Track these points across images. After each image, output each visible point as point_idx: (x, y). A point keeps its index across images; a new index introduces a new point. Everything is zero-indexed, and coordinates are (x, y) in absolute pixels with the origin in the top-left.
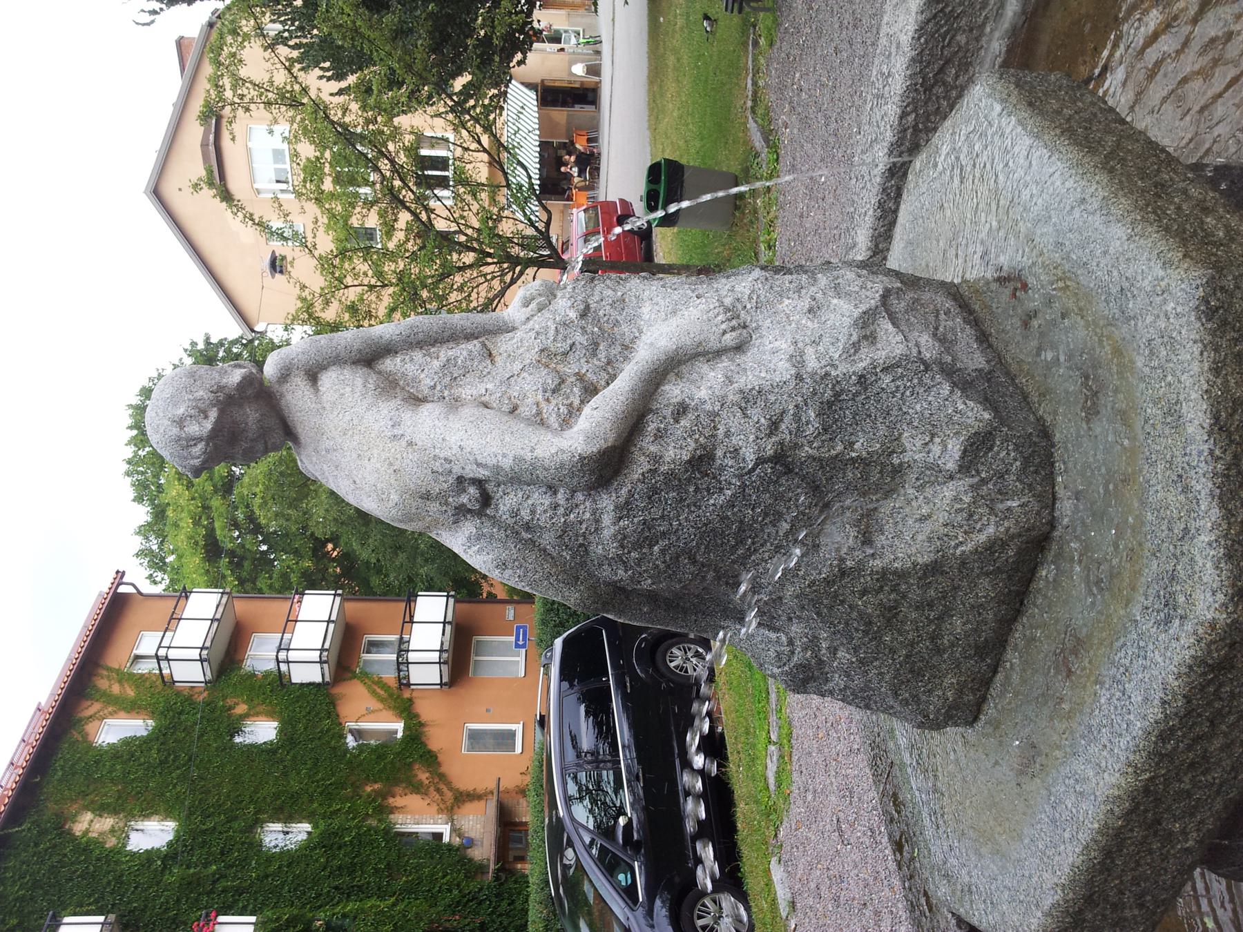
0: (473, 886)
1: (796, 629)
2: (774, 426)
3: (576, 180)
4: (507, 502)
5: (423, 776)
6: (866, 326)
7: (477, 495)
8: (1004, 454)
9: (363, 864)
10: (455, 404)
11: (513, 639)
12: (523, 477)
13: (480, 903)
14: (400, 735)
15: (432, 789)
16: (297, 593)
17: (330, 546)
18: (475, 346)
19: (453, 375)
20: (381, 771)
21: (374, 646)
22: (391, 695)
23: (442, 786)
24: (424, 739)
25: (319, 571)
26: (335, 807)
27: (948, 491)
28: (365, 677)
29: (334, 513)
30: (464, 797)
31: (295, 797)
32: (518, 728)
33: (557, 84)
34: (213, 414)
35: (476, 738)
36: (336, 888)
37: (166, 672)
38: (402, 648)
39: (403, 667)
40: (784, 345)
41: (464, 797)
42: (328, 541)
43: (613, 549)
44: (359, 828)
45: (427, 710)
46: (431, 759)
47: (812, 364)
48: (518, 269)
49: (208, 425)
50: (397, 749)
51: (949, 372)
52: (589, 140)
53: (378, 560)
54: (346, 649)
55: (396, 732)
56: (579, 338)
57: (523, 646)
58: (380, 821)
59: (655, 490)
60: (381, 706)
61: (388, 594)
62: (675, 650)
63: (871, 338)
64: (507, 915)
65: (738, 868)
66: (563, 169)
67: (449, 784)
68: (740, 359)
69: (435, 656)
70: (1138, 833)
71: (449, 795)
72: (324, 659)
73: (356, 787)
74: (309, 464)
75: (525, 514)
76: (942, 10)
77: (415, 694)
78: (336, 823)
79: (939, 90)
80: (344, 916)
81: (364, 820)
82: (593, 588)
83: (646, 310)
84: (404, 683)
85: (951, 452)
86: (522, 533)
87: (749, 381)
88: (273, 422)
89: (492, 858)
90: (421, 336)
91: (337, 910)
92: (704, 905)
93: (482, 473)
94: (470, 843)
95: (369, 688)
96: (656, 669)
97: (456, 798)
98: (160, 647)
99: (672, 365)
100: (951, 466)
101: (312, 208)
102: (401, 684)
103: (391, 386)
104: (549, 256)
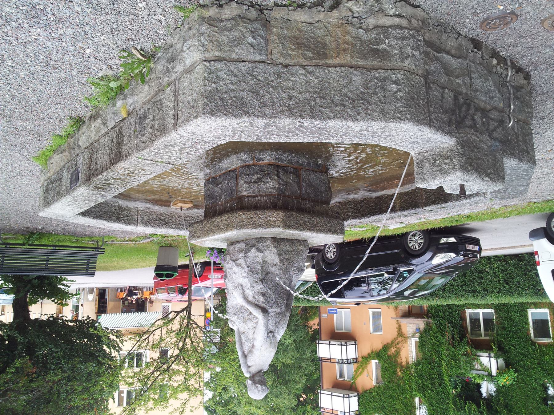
0: (434, 327)
1: (292, 273)
2: (256, 282)
3: (139, 296)
4: (271, 328)
5: (393, 350)
6: (239, 265)
7: (270, 333)
8: (260, 246)
9: (430, 374)
10: (254, 339)
11: (335, 315)
12: (267, 326)
13: (441, 324)
14: (377, 361)
15: (398, 346)
16: (320, 410)
17: (301, 399)
18: (242, 336)
19: (248, 339)
20: (392, 369)
21: (341, 375)
22: (361, 366)
23: (396, 342)
24: (378, 351)
25: (312, 403)
26: (408, 388)
27: (267, 254)
28: (354, 378)
29: (285, 395)
30: (400, 333)
31: (405, 405)
32: (371, 311)
33: (97, 306)
34: (257, 385)
35: (377, 328)
36: (440, 385)
38: (341, 362)
39: (349, 361)
40: (242, 279)
41: (400, 333)
42: (299, 399)
43: (279, 308)
44: (416, 377)
45: (366, 350)
46: (386, 347)
47: (245, 275)
48: (191, 322)
49: (259, 386)
50: (383, 362)
51: (246, 253)
52: (121, 291)
53: (305, 375)
54: (344, 387)
55: (376, 363)
56: (241, 315)
57: (336, 310)
58: (412, 368)
60: (366, 370)
61: (319, 370)
62: (328, 256)
63: (240, 264)
64: (444, 312)
65: (398, 235)
66: (134, 302)
67: (395, 339)
68: (244, 286)
69: (344, 348)
70: (317, 228)
71: (400, 339)
72: (347, 396)
73: (399, 379)
74: (266, 368)
75: (273, 324)
77: (360, 356)
78: (414, 387)
79: (166, 220)
80: (450, 381)
81: (412, 375)
82: (286, 311)
83: (235, 303)
84: (356, 361)
85: (260, 255)
86: (277, 325)
87: (249, 286)
88: (258, 375)
89: (423, 320)
91: (448, 384)
92: (422, 239)
93: (266, 333)
94: (418, 329)
95: (359, 376)
96: (334, 263)
97: (401, 336)
99: (246, 299)
100: (262, 254)
101: (171, 401)
102: (356, 362)
103: (250, 351)
104: (187, 311)
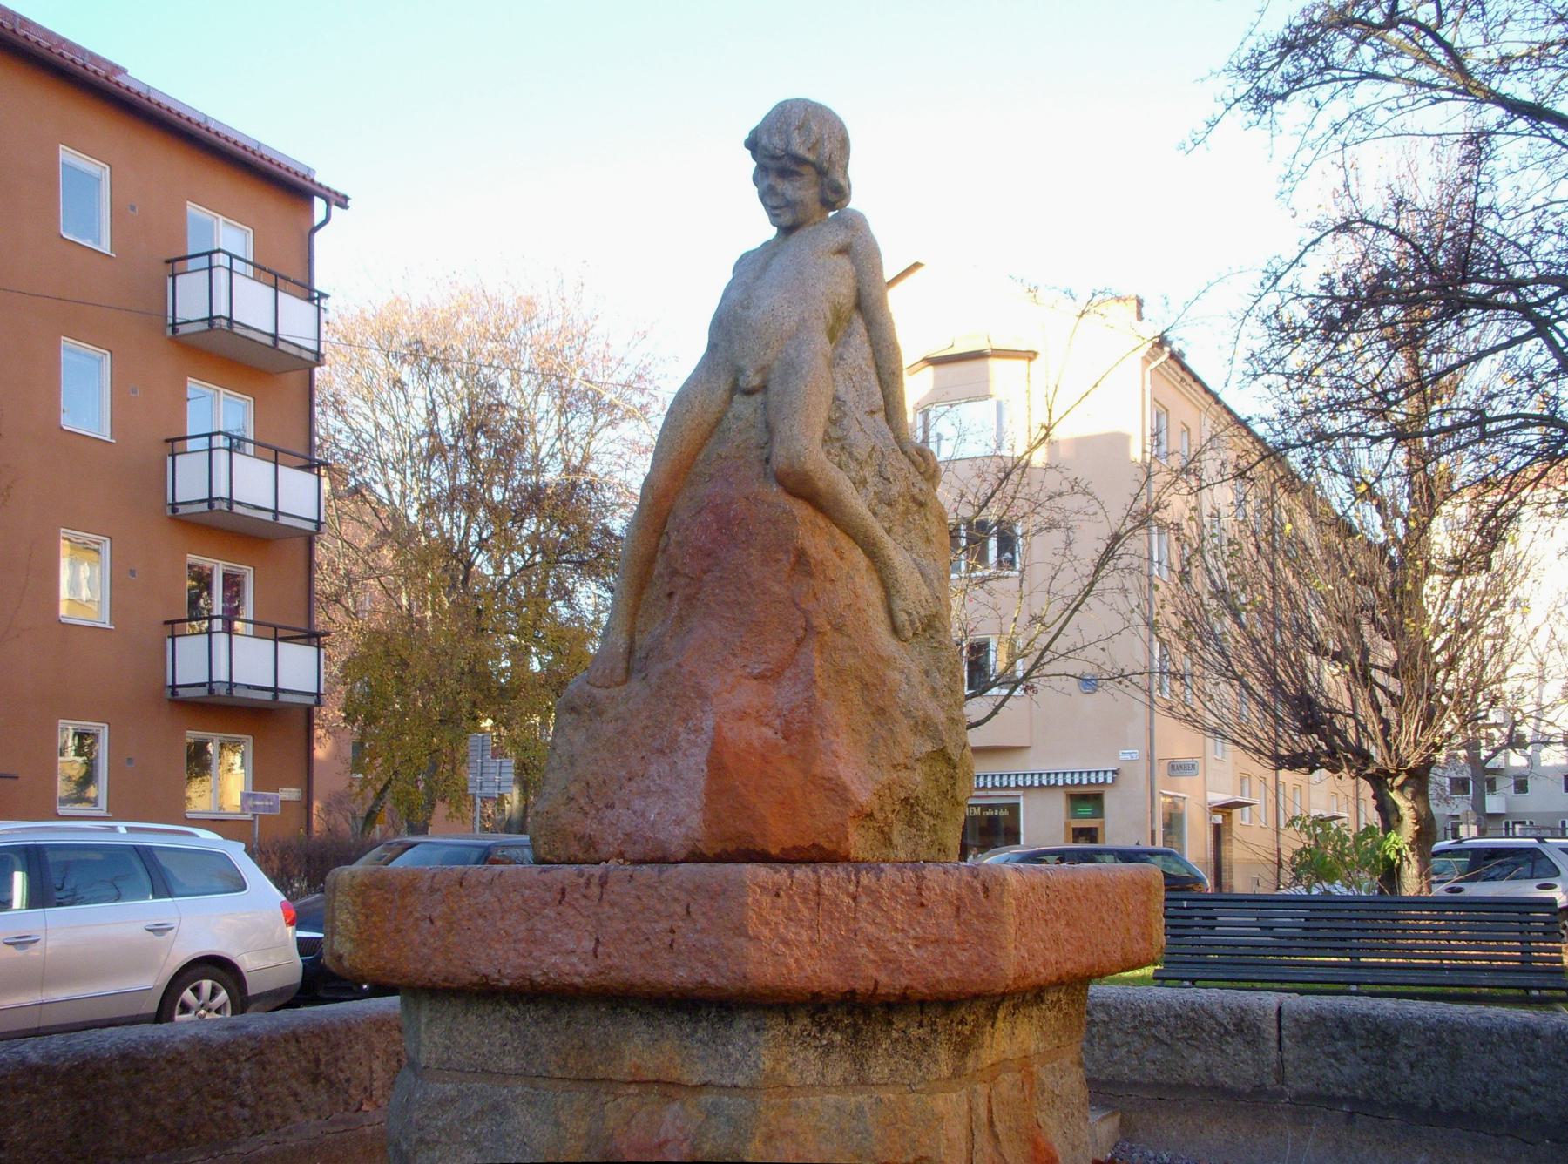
4: (744, 408)
37: (192, 264)
59: (775, 523)
72: (217, 505)
76: (1227, 1031)
90: (885, 352)
98: (231, 256)
